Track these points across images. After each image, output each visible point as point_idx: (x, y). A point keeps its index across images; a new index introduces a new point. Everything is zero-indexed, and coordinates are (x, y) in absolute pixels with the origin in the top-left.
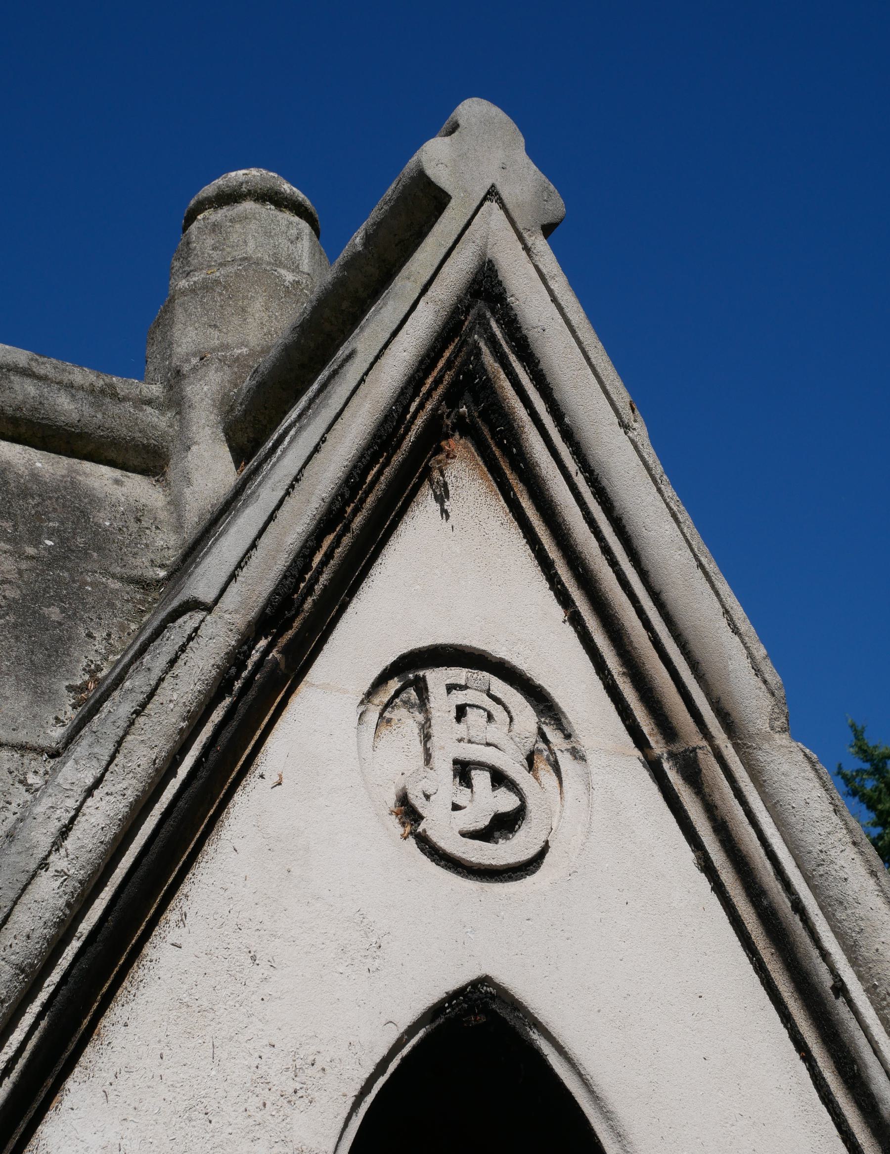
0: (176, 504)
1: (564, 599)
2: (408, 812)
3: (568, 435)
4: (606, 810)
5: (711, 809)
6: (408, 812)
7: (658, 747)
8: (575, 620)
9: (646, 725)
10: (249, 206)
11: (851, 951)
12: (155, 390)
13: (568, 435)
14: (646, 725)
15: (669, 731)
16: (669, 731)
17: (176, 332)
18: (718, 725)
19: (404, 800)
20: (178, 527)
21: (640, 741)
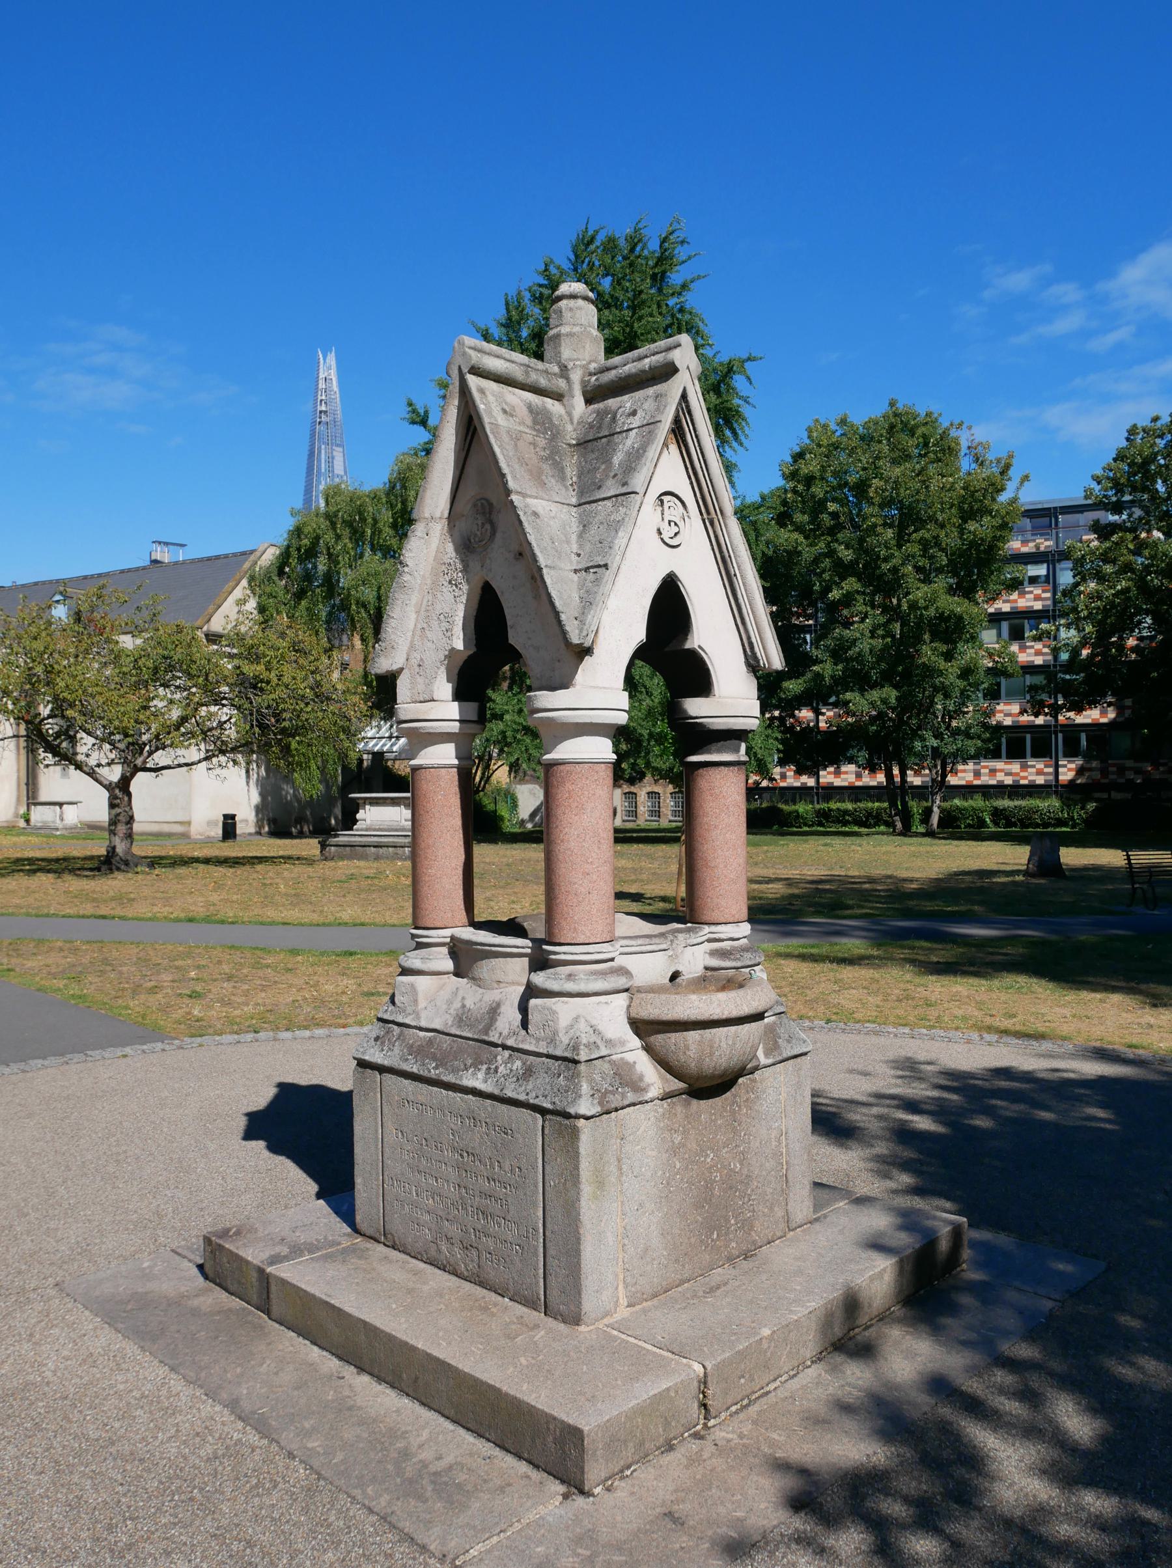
0: (569, 414)
1: (690, 478)
2: (659, 533)
3: (697, 436)
4: (694, 532)
5: (715, 532)
6: (659, 533)
7: (705, 516)
8: (691, 483)
9: (703, 511)
10: (580, 302)
11: (739, 567)
12: (556, 369)
13: (697, 436)
14: (703, 511)
15: (708, 513)
16: (708, 513)
17: (562, 349)
18: (1080, 850)
19: (659, 530)
20: (572, 423)
21: (701, 514)
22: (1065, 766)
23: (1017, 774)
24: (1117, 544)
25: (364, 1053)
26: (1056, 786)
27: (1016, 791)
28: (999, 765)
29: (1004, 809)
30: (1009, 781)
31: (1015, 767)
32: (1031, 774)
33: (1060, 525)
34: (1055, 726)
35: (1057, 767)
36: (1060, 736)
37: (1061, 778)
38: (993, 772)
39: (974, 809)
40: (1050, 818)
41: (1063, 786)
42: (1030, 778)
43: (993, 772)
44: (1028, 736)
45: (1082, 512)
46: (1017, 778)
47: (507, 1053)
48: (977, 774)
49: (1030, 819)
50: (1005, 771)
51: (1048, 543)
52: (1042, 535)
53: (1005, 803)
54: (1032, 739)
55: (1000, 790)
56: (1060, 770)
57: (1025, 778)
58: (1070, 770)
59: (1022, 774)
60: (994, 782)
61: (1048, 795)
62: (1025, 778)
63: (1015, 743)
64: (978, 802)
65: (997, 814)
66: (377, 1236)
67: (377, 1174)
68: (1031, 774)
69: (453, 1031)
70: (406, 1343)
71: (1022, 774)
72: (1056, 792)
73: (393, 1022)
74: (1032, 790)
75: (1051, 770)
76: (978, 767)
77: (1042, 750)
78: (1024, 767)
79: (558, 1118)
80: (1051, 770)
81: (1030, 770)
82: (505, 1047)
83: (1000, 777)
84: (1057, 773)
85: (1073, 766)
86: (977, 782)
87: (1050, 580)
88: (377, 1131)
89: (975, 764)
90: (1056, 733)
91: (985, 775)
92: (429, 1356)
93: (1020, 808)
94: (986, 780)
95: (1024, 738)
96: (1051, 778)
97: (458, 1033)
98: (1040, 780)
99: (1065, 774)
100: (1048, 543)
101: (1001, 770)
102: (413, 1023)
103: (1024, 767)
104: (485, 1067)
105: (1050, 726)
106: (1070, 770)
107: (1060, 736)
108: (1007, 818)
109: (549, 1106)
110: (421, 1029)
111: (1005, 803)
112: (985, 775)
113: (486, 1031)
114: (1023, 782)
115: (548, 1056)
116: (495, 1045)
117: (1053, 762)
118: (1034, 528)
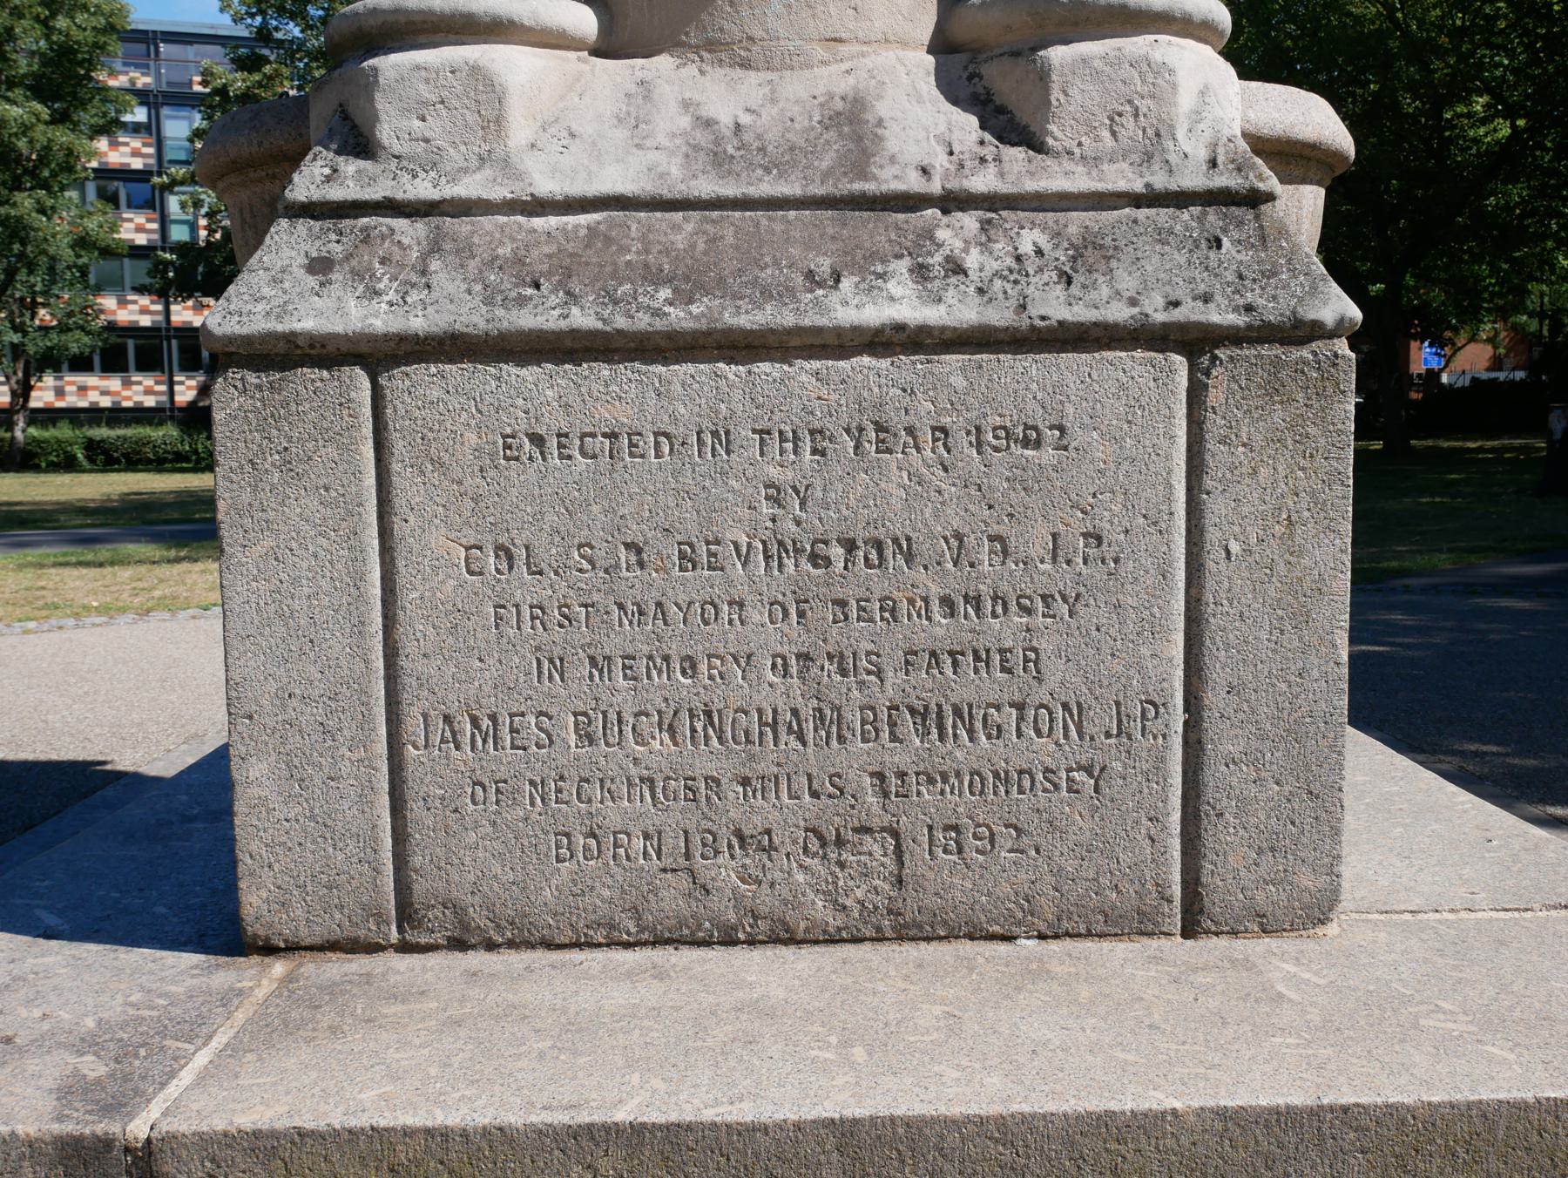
22: (182, 383)
23: (117, 393)
24: (270, 78)
25: (283, 312)
26: (172, 410)
27: (116, 415)
28: (91, 380)
29: (103, 441)
30: (106, 402)
31: (114, 383)
32: (136, 393)
33: (162, 56)
34: (168, 330)
35: (171, 384)
36: (174, 343)
37: (178, 398)
38: (83, 389)
39: (58, 441)
40: (166, 452)
41: (181, 409)
42: (137, 398)
43: (83, 389)
44: (131, 343)
45: (191, 43)
46: (117, 399)
47: (969, 221)
48: (60, 393)
49: (139, 453)
50: (99, 389)
51: (148, 80)
52: (137, 66)
53: (101, 432)
54: (137, 347)
55: (94, 415)
56: (177, 388)
57: (129, 398)
58: (189, 388)
59: (125, 393)
60: (84, 404)
61: (161, 423)
62: (129, 398)
63: (120, 351)
64: (63, 431)
65: (92, 446)
66: (367, 931)
67: (366, 720)
68: (136, 393)
69: (706, 187)
70: (1104, 1120)
71: (125, 393)
72: (172, 418)
73: (391, 207)
74: (139, 415)
75: (164, 388)
76: (59, 383)
77: (149, 361)
78: (127, 384)
79: (1266, 350)
80: (164, 388)
81: (135, 388)
82: (952, 202)
83: (93, 396)
84: (171, 393)
85: (193, 383)
86: (60, 404)
87: (151, 130)
88: (360, 578)
89: (57, 378)
90: (169, 339)
91: (71, 394)
92: (1230, 1120)
93: (125, 439)
94: (72, 400)
95: (124, 348)
96: (164, 398)
97: (730, 190)
98: (150, 402)
99: (183, 393)
100: (148, 80)
101: (95, 388)
102: (498, 193)
103: (127, 384)
104: (903, 266)
105: (159, 329)
106: (189, 388)
107: (174, 343)
108: (106, 452)
109: (1220, 315)
110: (539, 206)
111: (101, 432)
112: (71, 394)
113: (860, 162)
114: (126, 404)
115: (1137, 200)
116: (909, 202)
117: (165, 378)
118: (126, 55)
